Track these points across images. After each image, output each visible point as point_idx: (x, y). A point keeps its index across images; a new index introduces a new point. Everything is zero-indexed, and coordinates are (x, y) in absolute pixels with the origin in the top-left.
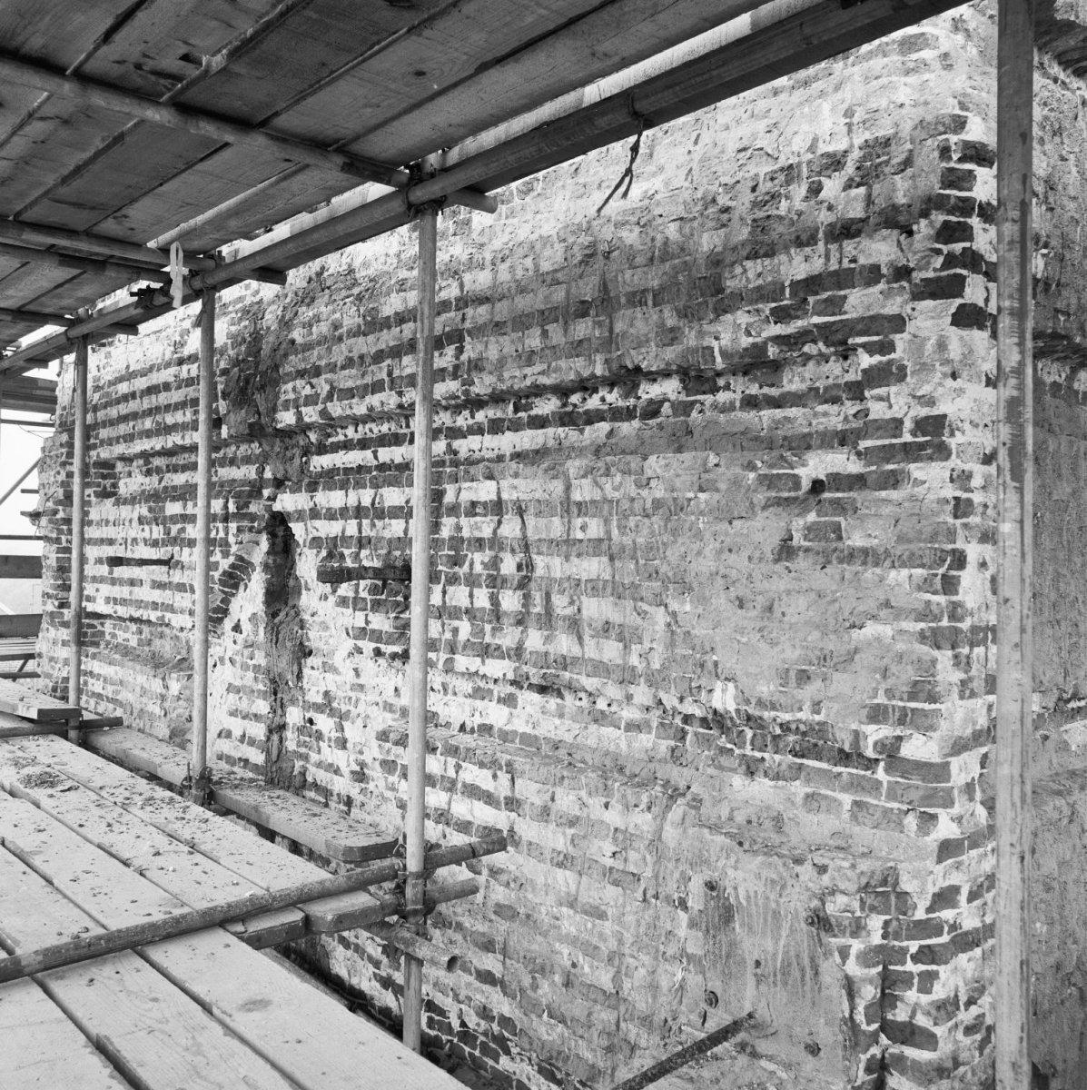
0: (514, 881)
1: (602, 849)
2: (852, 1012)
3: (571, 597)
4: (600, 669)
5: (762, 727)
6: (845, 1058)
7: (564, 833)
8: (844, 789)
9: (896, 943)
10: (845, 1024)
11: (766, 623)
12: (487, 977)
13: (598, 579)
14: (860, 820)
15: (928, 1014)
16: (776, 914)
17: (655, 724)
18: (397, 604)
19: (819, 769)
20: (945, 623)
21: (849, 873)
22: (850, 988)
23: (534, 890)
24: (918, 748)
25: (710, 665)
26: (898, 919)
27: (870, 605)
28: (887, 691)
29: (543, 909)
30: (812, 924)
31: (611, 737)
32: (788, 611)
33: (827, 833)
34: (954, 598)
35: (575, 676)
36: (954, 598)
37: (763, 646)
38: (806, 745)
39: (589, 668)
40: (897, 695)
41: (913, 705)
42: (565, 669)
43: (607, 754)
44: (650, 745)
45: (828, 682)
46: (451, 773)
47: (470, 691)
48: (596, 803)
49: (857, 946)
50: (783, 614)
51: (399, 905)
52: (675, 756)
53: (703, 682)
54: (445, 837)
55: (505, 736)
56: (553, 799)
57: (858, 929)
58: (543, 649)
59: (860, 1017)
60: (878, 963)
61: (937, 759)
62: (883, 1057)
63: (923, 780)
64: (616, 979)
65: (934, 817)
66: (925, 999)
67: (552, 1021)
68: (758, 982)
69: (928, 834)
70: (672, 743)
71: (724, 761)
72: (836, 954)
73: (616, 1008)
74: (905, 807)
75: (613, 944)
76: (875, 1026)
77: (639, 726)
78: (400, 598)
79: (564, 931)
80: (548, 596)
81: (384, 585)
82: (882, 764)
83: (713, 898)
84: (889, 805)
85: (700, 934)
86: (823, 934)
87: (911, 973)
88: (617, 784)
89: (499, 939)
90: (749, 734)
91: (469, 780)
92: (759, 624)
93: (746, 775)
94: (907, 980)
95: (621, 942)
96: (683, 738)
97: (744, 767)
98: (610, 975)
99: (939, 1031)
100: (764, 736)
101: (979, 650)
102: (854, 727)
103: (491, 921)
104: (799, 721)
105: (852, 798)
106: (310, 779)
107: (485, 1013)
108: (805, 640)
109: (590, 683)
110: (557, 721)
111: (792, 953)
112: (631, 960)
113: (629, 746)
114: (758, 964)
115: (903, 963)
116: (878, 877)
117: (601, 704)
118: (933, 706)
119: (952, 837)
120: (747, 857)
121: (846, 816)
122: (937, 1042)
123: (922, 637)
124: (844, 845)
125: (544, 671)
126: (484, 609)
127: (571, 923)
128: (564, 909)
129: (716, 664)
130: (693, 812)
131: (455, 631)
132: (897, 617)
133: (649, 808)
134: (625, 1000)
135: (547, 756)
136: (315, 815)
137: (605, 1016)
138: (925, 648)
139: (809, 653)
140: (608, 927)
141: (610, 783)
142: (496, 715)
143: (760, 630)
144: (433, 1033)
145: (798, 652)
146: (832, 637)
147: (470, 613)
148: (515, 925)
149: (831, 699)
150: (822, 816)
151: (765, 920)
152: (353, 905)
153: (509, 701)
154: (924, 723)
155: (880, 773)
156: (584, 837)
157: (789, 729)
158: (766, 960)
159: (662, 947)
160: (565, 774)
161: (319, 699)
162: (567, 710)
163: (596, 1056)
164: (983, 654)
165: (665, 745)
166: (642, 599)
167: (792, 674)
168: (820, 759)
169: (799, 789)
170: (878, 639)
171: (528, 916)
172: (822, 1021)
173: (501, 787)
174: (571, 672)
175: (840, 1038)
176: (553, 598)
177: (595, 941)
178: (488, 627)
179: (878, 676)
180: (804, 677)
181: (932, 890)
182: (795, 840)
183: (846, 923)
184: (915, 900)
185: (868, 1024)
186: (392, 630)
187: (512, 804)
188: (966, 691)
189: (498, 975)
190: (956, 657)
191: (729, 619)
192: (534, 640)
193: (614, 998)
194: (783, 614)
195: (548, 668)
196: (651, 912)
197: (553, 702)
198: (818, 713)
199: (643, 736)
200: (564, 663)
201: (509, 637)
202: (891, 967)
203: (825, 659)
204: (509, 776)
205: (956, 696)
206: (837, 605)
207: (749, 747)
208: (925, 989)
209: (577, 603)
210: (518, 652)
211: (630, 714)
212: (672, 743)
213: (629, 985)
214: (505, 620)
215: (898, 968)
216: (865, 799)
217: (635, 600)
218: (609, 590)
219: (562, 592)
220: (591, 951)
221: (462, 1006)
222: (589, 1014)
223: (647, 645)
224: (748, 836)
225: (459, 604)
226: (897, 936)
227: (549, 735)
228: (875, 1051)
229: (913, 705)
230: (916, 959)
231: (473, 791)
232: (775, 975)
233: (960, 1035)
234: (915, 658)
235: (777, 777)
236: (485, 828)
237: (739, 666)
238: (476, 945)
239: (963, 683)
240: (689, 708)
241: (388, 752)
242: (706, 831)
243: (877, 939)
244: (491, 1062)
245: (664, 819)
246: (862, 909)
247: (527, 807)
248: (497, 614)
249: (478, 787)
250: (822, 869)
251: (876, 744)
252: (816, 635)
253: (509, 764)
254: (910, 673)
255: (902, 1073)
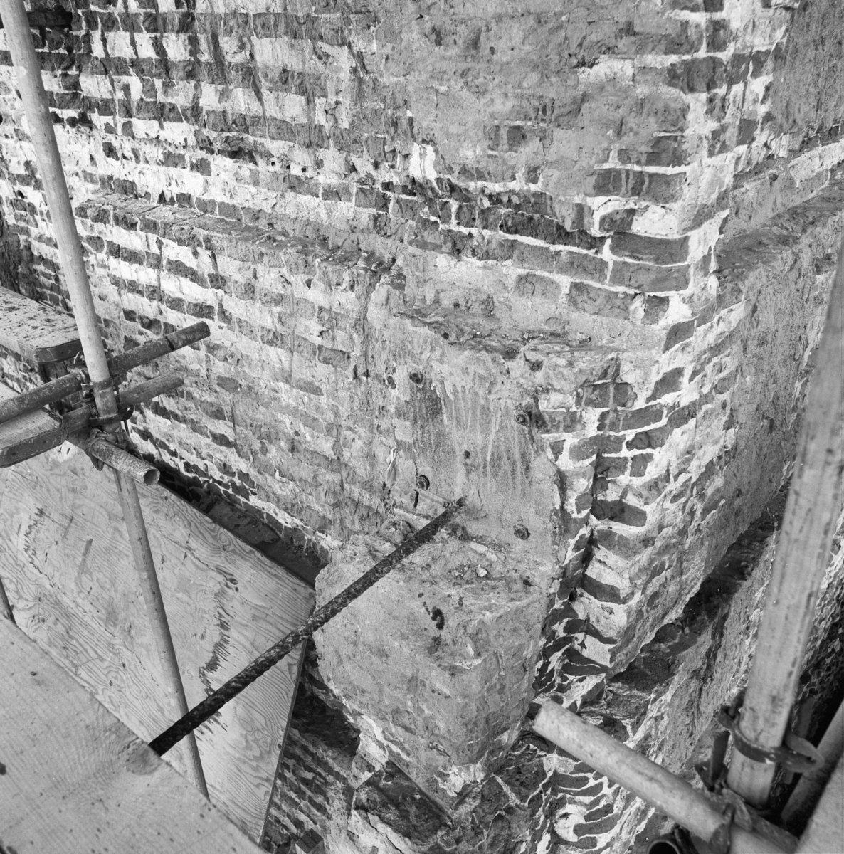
0: (232, 356)
1: (311, 328)
2: (563, 503)
3: (240, 39)
4: (284, 130)
5: (467, 199)
6: (554, 543)
7: (270, 312)
8: (562, 270)
9: (612, 433)
10: (556, 514)
11: (470, 64)
12: (221, 440)
13: (268, 13)
14: (580, 305)
15: (640, 495)
16: (485, 410)
17: (354, 190)
18: (61, 58)
19: (535, 247)
20: (702, 53)
21: (566, 372)
22: (562, 481)
23: (250, 365)
24: (655, 222)
25: (404, 124)
26: (616, 411)
27: (604, 32)
28: (621, 152)
29: (262, 383)
30: (524, 422)
31: (308, 206)
32: (501, 45)
33: (542, 318)
34: (718, 16)
35: (259, 140)
36: (718, 16)
37: (467, 96)
38: (519, 218)
39: (273, 130)
40: (634, 156)
41: (652, 169)
42: (247, 131)
43: (308, 223)
44: (350, 214)
45: (547, 142)
46: (154, 249)
47: (161, 157)
48: (298, 280)
49: (570, 440)
50: (492, 50)
51: (91, 415)
52: (378, 224)
53: (397, 145)
54: (161, 313)
55: (206, 206)
56: (255, 277)
57: (572, 422)
58: (219, 107)
59: (571, 506)
60: (592, 453)
61: (675, 236)
62: (592, 535)
63: (657, 260)
64: (335, 447)
65: (664, 301)
66: (637, 482)
67: (284, 479)
68: (468, 471)
69: (656, 321)
70: (374, 211)
71: (429, 236)
72: (549, 450)
73: (339, 471)
74: (632, 292)
75: (330, 417)
76: (586, 512)
77: (337, 193)
78: (62, 51)
79: (284, 403)
80: (215, 38)
81: (43, 33)
82: (608, 242)
83: (419, 390)
84: (613, 289)
85: (408, 423)
86: (535, 430)
87: (626, 459)
88: (318, 260)
89: (227, 408)
90: (454, 205)
91: (173, 258)
92: (462, 66)
93: (452, 254)
94: (620, 465)
95: (336, 415)
96: (385, 206)
97: (449, 244)
98: (330, 444)
99: (647, 509)
100: (471, 208)
101: (737, 88)
102: (577, 200)
103: (216, 392)
104: (512, 192)
105: (572, 280)
106: (36, 253)
107: (225, 468)
108: (520, 86)
109: (276, 147)
110: (253, 190)
111: (502, 448)
112: (348, 433)
113: (329, 216)
114: (467, 455)
115: (618, 450)
116: (599, 371)
117: (295, 170)
118: (677, 170)
119: (682, 321)
120: (452, 352)
121: (563, 299)
122: (645, 518)
123: (672, 76)
124: (559, 331)
125: (226, 134)
126: (150, 59)
127: (289, 396)
128: (281, 385)
129: (411, 121)
130: (397, 292)
131: (126, 89)
132: (641, 50)
133: (352, 287)
134: (346, 465)
135: (248, 229)
136: (12, 309)
137: (330, 477)
138: (675, 92)
139: (525, 103)
140: (323, 401)
141: (310, 258)
142: (191, 183)
143: (464, 74)
144: (191, 475)
145: (510, 104)
146: (554, 79)
147: (136, 64)
148: (239, 396)
149: (550, 164)
150: (537, 300)
151: (474, 415)
152: (28, 431)
153: (201, 167)
154: (659, 190)
155: (606, 254)
156: (291, 315)
157: (499, 201)
158: (476, 452)
159: (376, 421)
160: (264, 250)
161: (22, 171)
162: (261, 177)
163: (324, 510)
164: (740, 94)
165: (366, 214)
166: (321, 37)
167: (504, 133)
168: (536, 236)
169: (512, 269)
170: (613, 80)
171: (250, 388)
172: (532, 510)
173: (203, 264)
174: (253, 135)
175: (551, 526)
176: (220, 39)
177: (313, 414)
178: (158, 83)
179: (610, 133)
180: (518, 136)
181: (655, 378)
182: (506, 325)
183: (560, 418)
184: (635, 390)
185: (579, 512)
186: (62, 91)
187: (217, 281)
188: (717, 143)
189: (231, 439)
190: (711, 100)
191: (424, 60)
192: (209, 98)
193: (337, 463)
194: (492, 50)
195: (229, 130)
196: (363, 388)
197: (246, 168)
198: (535, 181)
199: (342, 204)
200: (245, 123)
201: (181, 94)
202: (605, 455)
203: (544, 111)
204: (209, 252)
205: (704, 153)
206: (562, 34)
207: (454, 221)
208: (638, 473)
209: (248, 46)
210: (194, 113)
211: (326, 179)
212: (374, 211)
213: (349, 454)
214: (174, 73)
215: (613, 455)
216: (586, 282)
217: (313, 39)
218: (282, 27)
219: (229, 32)
220: (312, 422)
221: (206, 462)
222: (315, 477)
223: (332, 98)
224: (461, 325)
225: (122, 55)
226: (613, 427)
227: (246, 204)
228: (585, 531)
229: (652, 169)
230: (630, 445)
231: (178, 268)
232: (485, 466)
233: (667, 504)
234: (660, 106)
235: (486, 256)
236: (196, 305)
237: (438, 125)
238: (207, 413)
239: (715, 135)
240: (384, 175)
241: (91, 227)
242: (408, 322)
243: (592, 431)
244: (243, 499)
245: (368, 296)
246: (578, 404)
247: (231, 284)
248: (165, 65)
249: (182, 264)
250: (536, 366)
251: (603, 220)
252: (534, 77)
253: (207, 240)
254: (652, 128)
255: (609, 547)
